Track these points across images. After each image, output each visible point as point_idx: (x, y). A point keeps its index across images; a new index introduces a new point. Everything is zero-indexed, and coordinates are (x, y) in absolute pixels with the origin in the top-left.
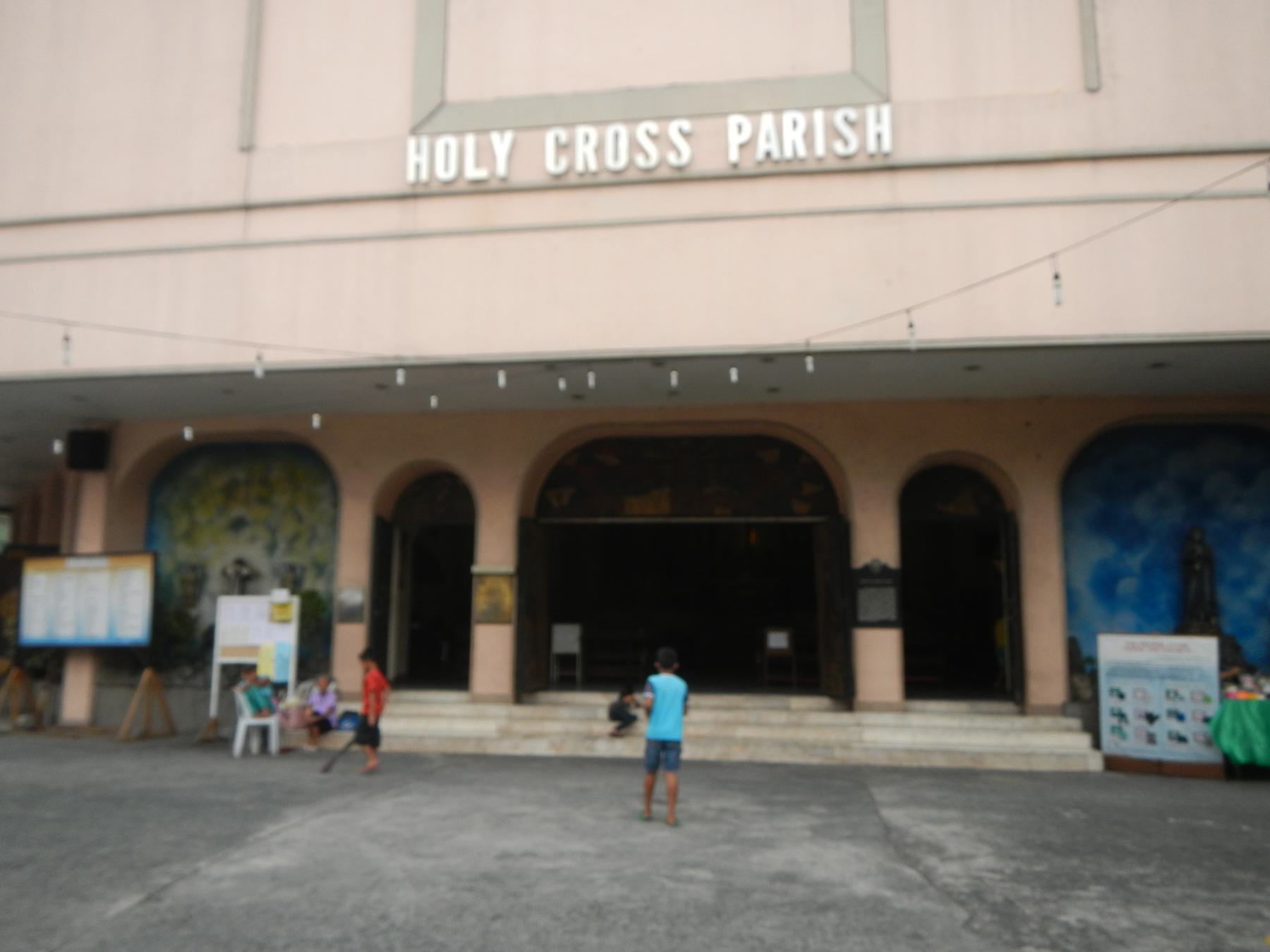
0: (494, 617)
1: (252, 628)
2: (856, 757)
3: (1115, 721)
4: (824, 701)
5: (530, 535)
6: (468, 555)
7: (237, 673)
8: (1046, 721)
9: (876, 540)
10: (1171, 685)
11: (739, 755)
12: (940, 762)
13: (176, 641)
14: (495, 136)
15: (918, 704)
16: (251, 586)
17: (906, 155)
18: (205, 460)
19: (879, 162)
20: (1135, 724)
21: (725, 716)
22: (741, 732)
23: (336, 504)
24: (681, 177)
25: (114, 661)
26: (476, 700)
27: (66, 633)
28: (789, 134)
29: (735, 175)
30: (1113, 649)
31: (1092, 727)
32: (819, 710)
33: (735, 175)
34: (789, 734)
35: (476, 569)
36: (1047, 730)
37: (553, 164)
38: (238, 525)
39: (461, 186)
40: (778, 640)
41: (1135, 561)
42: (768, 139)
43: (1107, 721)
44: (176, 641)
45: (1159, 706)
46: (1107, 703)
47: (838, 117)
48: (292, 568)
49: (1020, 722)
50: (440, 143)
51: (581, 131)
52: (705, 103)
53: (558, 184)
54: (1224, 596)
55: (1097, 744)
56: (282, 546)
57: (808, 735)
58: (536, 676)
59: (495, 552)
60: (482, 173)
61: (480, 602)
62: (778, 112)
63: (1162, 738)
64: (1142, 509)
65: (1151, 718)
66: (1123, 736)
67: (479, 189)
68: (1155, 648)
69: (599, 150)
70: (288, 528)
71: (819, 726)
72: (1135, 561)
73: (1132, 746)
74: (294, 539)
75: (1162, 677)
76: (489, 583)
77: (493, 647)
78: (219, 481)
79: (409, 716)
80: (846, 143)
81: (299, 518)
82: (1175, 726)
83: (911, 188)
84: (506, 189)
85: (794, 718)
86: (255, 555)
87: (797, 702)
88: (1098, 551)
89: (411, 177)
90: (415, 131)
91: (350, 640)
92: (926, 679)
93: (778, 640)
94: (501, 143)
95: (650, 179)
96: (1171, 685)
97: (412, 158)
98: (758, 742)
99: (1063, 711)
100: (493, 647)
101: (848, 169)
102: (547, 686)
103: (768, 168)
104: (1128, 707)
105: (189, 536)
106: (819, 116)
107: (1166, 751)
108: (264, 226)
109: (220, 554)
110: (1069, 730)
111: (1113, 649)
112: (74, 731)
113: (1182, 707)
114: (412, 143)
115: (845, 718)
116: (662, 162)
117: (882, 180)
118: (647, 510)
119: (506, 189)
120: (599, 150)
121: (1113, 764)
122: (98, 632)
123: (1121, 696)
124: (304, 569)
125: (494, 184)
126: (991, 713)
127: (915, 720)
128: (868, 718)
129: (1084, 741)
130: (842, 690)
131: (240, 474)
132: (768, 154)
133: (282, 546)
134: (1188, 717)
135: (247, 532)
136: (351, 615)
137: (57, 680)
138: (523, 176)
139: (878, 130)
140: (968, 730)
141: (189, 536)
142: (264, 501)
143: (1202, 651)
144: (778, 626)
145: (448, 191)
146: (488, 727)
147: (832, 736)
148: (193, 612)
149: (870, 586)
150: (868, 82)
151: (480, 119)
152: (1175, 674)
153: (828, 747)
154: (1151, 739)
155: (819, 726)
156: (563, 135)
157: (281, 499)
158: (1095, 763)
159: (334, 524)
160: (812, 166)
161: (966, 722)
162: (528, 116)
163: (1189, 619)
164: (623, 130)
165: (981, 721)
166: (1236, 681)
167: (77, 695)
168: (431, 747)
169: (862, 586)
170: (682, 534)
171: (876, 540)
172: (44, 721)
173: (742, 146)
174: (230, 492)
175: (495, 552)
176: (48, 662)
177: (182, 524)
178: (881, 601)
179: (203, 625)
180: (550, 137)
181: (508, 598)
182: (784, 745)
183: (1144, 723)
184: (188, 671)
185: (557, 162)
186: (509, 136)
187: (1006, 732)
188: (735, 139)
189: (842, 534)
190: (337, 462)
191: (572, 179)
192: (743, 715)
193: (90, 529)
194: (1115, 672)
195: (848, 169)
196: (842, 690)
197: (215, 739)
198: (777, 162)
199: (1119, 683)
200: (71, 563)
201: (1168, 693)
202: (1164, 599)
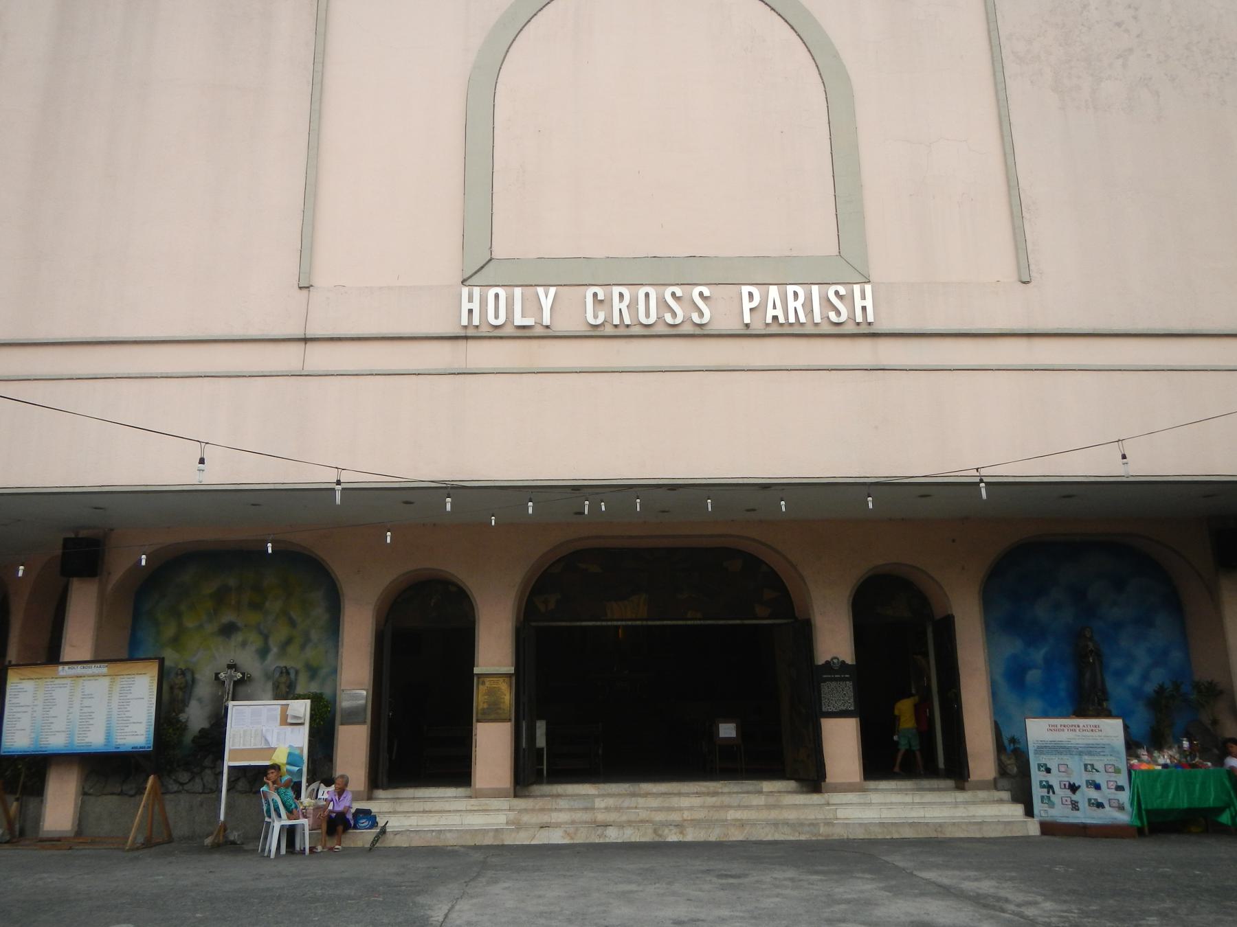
0: (492, 715)
1: (265, 730)
2: (839, 833)
3: (1044, 792)
4: (792, 784)
5: (532, 642)
6: (470, 661)
7: (252, 778)
8: (982, 794)
9: (835, 641)
10: (1088, 759)
11: (737, 835)
12: (908, 833)
13: (184, 749)
14: (540, 290)
15: (872, 784)
16: (242, 690)
18: (197, 571)
20: (1061, 793)
21: (710, 800)
22: (732, 815)
24: (702, 333)
25: (106, 769)
26: (477, 795)
27: (56, 742)
28: (789, 303)
29: (746, 334)
30: (1039, 731)
31: (1023, 796)
33: (746, 334)
34: (774, 815)
35: (476, 670)
36: (984, 802)
37: (592, 316)
38: (228, 630)
39: (508, 331)
40: (727, 730)
41: (1039, 655)
42: (775, 307)
43: (1037, 793)
44: (184, 749)
45: (1079, 778)
46: (1037, 776)
48: (285, 671)
49: (961, 796)
52: (726, 274)
53: (594, 334)
54: (1111, 684)
55: (1029, 812)
56: (275, 650)
57: (791, 815)
58: (530, 772)
59: (494, 654)
60: (529, 321)
61: (480, 699)
63: (1083, 805)
65: (1074, 788)
66: (1052, 805)
67: (524, 334)
68: (1073, 729)
69: (633, 306)
70: (281, 633)
71: (795, 806)
72: (1039, 655)
73: (1060, 813)
74: (289, 641)
75: (1080, 754)
76: (488, 683)
77: (492, 745)
78: (209, 588)
80: (838, 313)
81: (293, 623)
82: (1093, 794)
83: (889, 352)
84: (549, 335)
85: (771, 800)
86: (248, 660)
87: (767, 786)
88: (1012, 646)
89: (465, 322)
91: (353, 745)
92: (881, 762)
93: (727, 730)
94: (546, 298)
95: (674, 334)
96: (1088, 759)
97: (466, 306)
98: (753, 823)
99: (995, 785)
100: (492, 745)
101: (838, 334)
102: (539, 779)
103: (775, 329)
104: (1053, 780)
105: (176, 642)
107: (1087, 816)
108: (320, 357)
109: (210, 659)
110: (1001, 801)
111: (1039, 731)
112: (56, 841)
113: (1098, 778)
114: (465, 290)
115: (815, 798)
116: (688, 319)
117: (866, 344)
118: (626, 614)
119: (549, 335)
120: (633, 306)
121: (1048, 828)
122: (95, 739)
123: (1048, 771)
124: (297, 672)
125: (539, 331)
126: (932, 790)
127: (875, 798)
128: (836, 798)
129: (1018, 810)
130: (813, 778)
131: (232, 582)
132: (775, 318)
133: (275, 650)
134: (1104, 786)
135: (238, 638)
136: (352, 717)
137: (38, 790)
138: (561, 327)
139: (864, 303)
141: (176, 642)
142: (256, 606)
143: (1111, 730)
144: (727, 719)
145: (496, 335)
146: (499, 820)
147: (811, 815)
148: (183, 717)
149: (831, 680)
150: (850, 265)
151: (530, 275)
152: (1090, 750)
153: (814, 824)
154: (1075, 806)
155: (795, 806)
157: (274, 605)
158: (1033, 828)
159: (334, 629)
160: (809, 330)
161: (908, 799)
162: (571, 274)
163: (1087, 702)
165: (930, 797)
167: (60, 807)
168: (451, 840)
170: (669, 637)
171: (835, 641)
172: (23, 833)
174: (220, 598)
175: (494, 654)
176: (29, 773)
177: (170, 631)
178: (839, 694)
180: (590, 292)
181: (507, 697)
182: (776, 824)
183: (1068, 792)
184: (184, 777)
185: (596, 317)
186: (552, 290)
187: (956, 805)
189: (804, 632)
190: (339, 570)
192: (726, 800)
193: (79, 637)
194: (1043, 749)
195: (838, 334)
196: (813, 778)
197: (238, 842)
198: (782, 325)
199: (1044, 759)
200: (63, 670)
201: (1086, 766)
202: (1063, 686)
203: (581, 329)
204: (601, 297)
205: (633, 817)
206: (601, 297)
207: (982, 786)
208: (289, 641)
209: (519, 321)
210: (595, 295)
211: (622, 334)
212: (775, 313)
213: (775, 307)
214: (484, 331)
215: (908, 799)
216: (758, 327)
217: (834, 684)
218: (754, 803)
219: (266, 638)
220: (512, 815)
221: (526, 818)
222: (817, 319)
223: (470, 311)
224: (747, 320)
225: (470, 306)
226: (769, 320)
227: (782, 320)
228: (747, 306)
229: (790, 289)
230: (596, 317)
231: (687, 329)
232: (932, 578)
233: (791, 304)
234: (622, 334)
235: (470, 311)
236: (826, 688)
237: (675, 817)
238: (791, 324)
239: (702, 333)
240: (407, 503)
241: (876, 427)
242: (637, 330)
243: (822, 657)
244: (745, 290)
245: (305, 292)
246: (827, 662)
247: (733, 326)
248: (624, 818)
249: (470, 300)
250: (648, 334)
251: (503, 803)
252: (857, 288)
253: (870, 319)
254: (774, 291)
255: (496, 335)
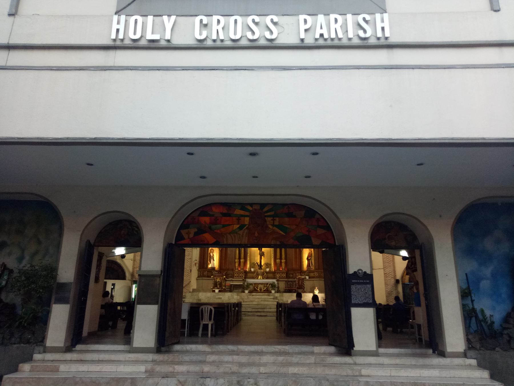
4: (332, 349)
8: (458, 361)
17: (394, 39)
19: (382, 42)
23: (61, 235)
32: (331, 354)
37: (199, 34)
39: (143, 43)
41: (488, 271)
42: (321, 28)
47: (360, 18)
50: (132, 19)
51: (215, 18)
53: (200, 46)
60: (156, 37)
62: (327, 14)
64: (488, 244)
71: (334, 365)
72: (488, 271)
74: (36, 253)
79: (93, 362)
80: (365, 31)
81: (39, 243)
84: (170, 47)
88: (471, 266)
89: (113, 36)
90: (116, 13)
94: (168, 22)
95: (254, 46)
97: (115, 27)
99: (465, 355)
103: (321, 42)
106: (349, 17)
110: (470, 366)
114: (116, 17)
115: (347, 359)
119: (170, 47)
125: (163, 43)
132: (322, 35)
138: (177, 41)
140: (415, 366)
156: (205, 20)
159: (58, 247)
160: (345, 41)
161: (412, 361)
164: (239, 19)
166: (19, 273)
169: (354, 284)
173: (306, 30)
179: (386, 251)
180: (198, 19)
185: (201, 34)
188: (303, 27)
191: (209, 43)
203: (191, 42)
204: (205, 22)
205: (227, 370)
206: (205, 22)
207: (455, 355)
208: (36, 253)
209: (150, 36)
210: (201, 21)
211: (218, 46)
212: (322, 32)
213: (321, 28)
214: (127, 42)
215: (398, 361)
216: (309, 40)
217: (359, 286)
218: (308, 362)
219: (23, 251)
220: (149, 366)
221: (158, 368)
222: (351, 35)
223: (118, 30)
224: (302, 36)
225: (118, 27)
226: (317, 36)
227: (326, 36)
228: (303, 27)
229: (332, 17)
230: (201, 34)
231: (263, 42)
232: (422, 223)
233: (333, 26)
234: (218, 46)
235: (118, 30)
236: (353, 288)
237: (254, 370)
238: (332, 39)
239: (272, 46)
240: (88, 164)
241: (391, 106)
242: (228, 43)
243: (352, 269)
244: (302, 17)
245: (12, 18)
246: (355, 272)
247: (293, 40)
248: (222, 370)
249: (118, 23)
250: (235, 46)
251: (150, 357)
252: (378, 16)
253: (387, 34)
254: (321, 18)
255: (135, 46)
